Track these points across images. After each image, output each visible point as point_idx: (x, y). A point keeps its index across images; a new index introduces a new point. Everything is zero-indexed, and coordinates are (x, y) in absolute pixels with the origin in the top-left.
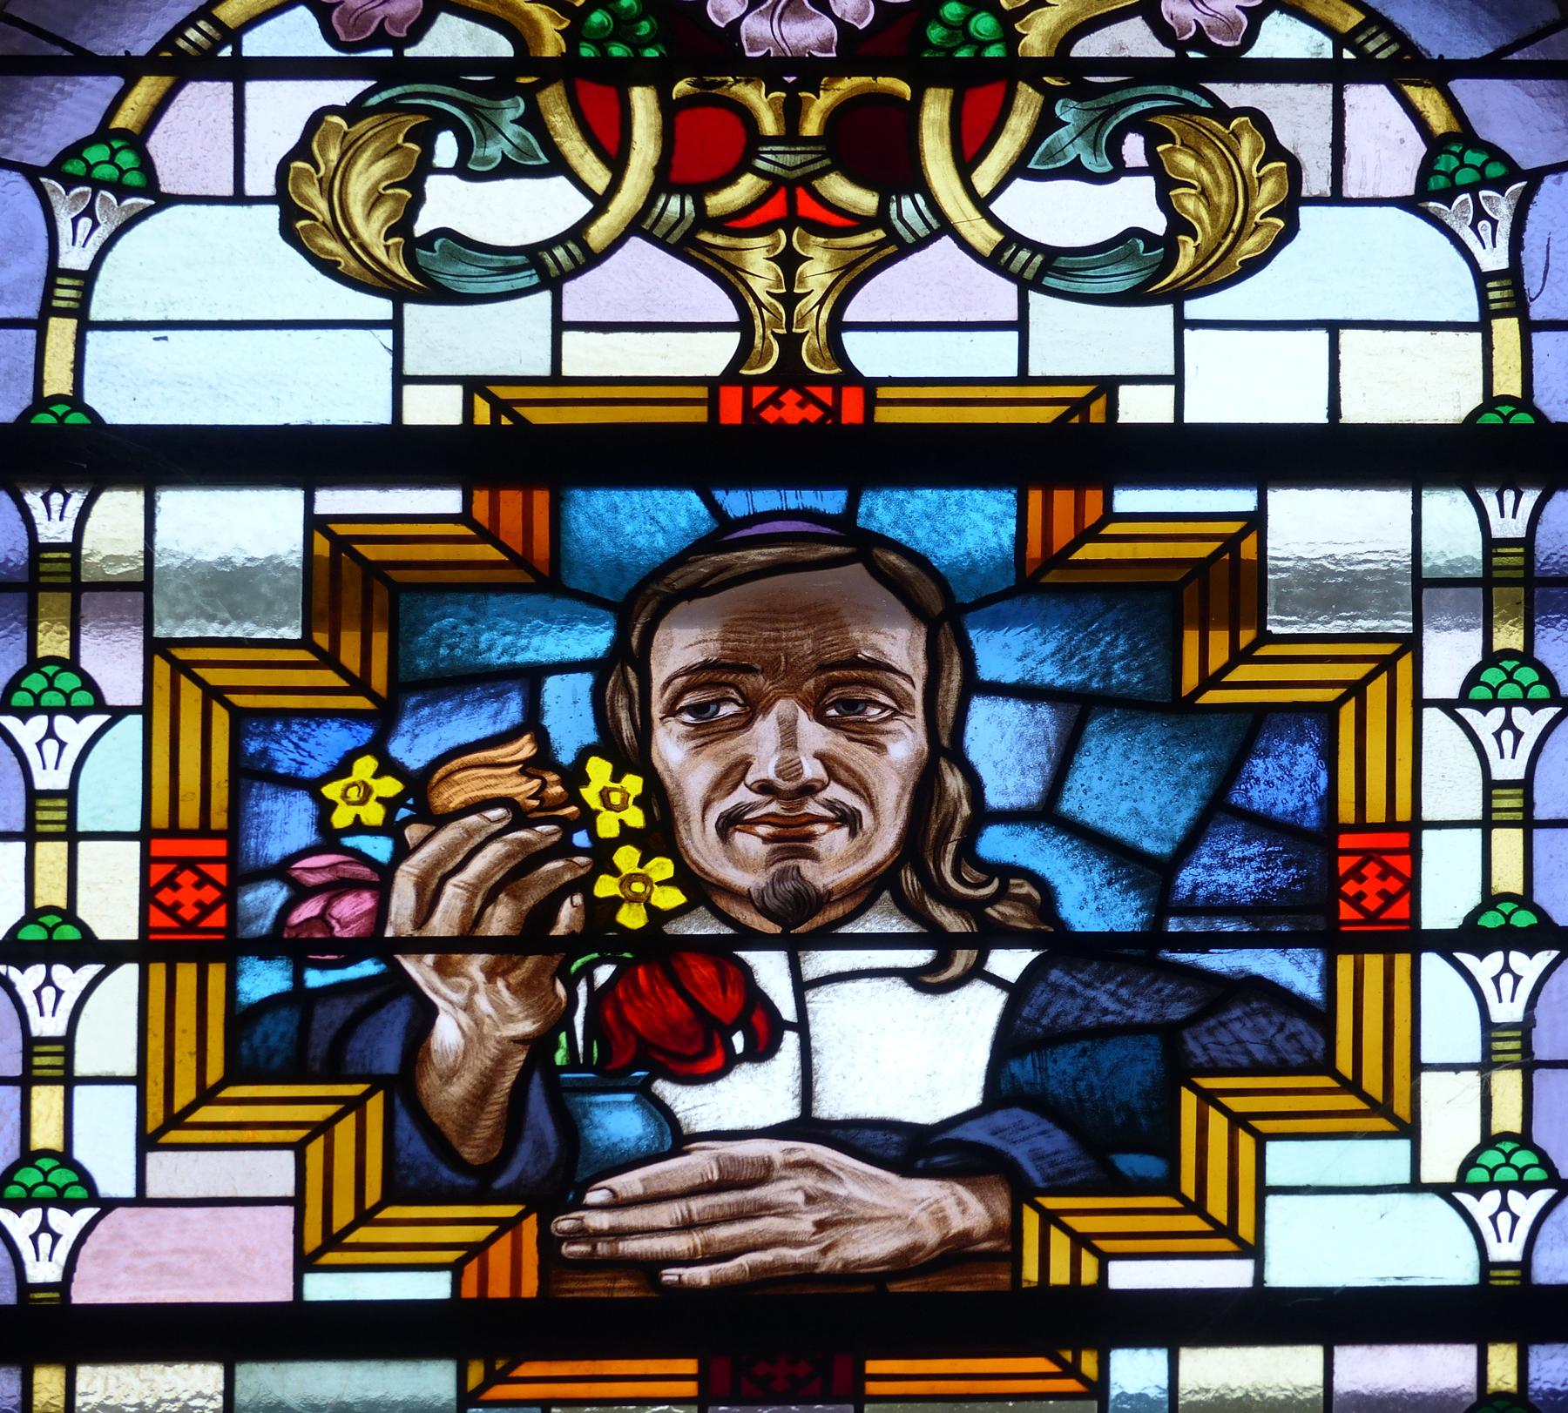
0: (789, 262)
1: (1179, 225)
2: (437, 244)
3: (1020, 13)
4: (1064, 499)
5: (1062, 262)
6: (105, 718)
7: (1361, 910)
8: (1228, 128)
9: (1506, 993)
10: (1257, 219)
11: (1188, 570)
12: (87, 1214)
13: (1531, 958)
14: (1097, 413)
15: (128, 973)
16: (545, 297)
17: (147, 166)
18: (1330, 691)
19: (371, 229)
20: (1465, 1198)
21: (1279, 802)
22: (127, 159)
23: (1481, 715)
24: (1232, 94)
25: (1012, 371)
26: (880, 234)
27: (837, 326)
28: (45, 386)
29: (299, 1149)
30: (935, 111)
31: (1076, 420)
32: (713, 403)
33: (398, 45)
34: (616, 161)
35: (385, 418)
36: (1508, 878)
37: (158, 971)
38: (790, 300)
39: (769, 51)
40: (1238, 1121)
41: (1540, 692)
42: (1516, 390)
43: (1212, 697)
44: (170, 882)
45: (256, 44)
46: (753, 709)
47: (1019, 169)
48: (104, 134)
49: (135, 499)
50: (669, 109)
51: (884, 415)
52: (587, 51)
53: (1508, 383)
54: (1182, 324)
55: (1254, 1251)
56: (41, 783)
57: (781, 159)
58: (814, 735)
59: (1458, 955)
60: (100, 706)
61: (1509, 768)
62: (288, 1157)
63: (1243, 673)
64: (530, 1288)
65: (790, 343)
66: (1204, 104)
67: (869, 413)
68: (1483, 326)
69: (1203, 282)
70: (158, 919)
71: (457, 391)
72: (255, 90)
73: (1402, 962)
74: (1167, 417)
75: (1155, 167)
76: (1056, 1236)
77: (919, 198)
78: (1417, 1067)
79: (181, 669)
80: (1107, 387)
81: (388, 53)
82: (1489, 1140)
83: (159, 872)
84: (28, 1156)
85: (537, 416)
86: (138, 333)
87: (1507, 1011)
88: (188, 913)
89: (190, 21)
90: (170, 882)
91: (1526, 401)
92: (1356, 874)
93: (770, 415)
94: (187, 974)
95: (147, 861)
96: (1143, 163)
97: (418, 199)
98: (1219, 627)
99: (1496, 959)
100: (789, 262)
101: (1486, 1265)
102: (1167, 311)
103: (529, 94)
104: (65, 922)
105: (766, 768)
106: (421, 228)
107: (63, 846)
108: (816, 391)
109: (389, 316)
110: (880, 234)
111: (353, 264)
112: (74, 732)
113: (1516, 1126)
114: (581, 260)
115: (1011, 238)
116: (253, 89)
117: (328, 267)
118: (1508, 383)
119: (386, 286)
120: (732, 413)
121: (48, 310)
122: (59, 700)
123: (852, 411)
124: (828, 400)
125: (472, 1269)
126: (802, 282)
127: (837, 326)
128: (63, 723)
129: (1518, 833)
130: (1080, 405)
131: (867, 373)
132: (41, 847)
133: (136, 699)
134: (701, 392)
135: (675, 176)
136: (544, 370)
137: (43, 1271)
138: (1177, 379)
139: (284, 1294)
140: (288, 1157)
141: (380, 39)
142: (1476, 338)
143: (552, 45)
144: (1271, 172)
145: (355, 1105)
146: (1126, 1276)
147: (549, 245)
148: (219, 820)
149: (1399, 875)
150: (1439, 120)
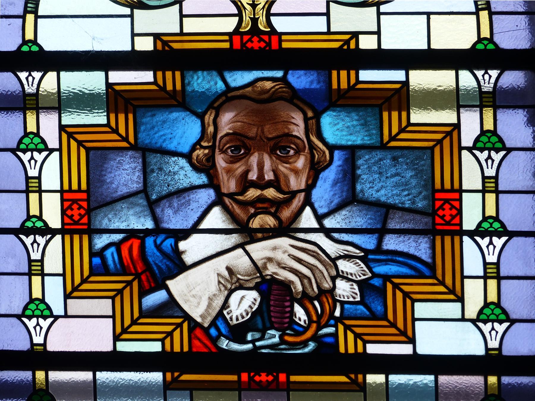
4: (344, 74)
6: (47, 152)
7: (444, 220)
9: (493, 337)
11: (384, 100)
12: (50, 320)
14: (352, 45)
15: (58, 238)
16: (177, 6)
18: (430, 143)
23: (480, 153)
25: (325, 30)
27: (269, 15)
28: (28, 129)
29: (113, 298)
31: (176, 374)
35: (129, 48)
36: (491, 211)
37: (67, 238)
40: (406, 295)
41: (503, 317)
42: (495, 300)
44: (70, 208)
46: (248, 153)
49: (55, 73)
51: (285, 45)
53: (485, 33)
54: (379, 14)
55: (412, 341)
56: (30, 175)
60: (52, 315)
61: (492, 258)
62: (110, 301)
63: (120, 286)
65: (255, 21)
67: (280, 45)
68: (476, 13)
71: (151, 38)
73: (457, 239)
74: (375, 46)
78: (463, 277)
79: (70, 136)
80: (355, 35)
83: (66, 204)
85: (175, 46)
90: (70, 208)
91: (491, 40)
93: (249, 45)
95: (63, 200)
98: (395, 110)
99: (487, 239)
101: (487, 349)
102: (375, 8)
107: (40, 277)
109: (130, 13)
112: (39, 157)
118: (485, 33)
120: (237, 45)
121: (26, 12)
123: (275, 46)
125: (168, 341)
127: (269, 15)
129: (494, 195)
130: (347, 42)
132: (33, 278)
134: (226, 38)
136: (178, 31)
137: (38, 340)
138: (378, 33)
142: (474, 17)
146: (372, 349)
148: (84, 186)
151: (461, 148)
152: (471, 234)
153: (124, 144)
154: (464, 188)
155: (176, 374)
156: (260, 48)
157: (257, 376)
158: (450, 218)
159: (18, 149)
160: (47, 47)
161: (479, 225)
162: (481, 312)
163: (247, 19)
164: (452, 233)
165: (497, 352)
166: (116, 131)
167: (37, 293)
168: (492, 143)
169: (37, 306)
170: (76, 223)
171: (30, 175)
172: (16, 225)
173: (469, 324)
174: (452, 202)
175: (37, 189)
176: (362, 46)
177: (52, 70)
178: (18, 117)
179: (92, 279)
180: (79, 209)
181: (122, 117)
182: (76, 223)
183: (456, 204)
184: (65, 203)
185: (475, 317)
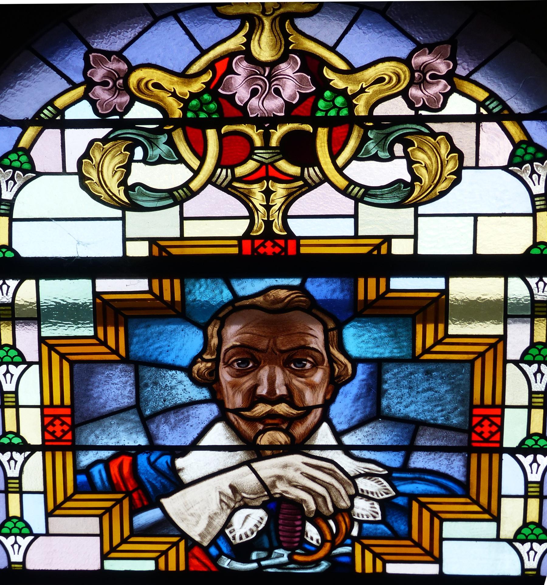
0: (268, 193)
1: (416, 178)
2: (136, 189)
3: (355, 95)
4: (372, 282)
5: (372, 192)
6: (25, 366)
8: (435, 140)
10: (446, 175)
12: (30, 538)
14: (384, 250)
17: (31, 161)
19: (113, 183)
20: (518, 545)
21: (358, 438)
22: (24, 158)
24: (437, 127)
25: (352, 234)
26: (301, 183)
27: (285, 217)
29: (100, 517)
30: (322, 134)
33: (122, 114)
34: (202, 157)
37: (49, 455)
38: (268, 207)
39: (258, 114)
43: (427, 357)
44: (51, 423)
45: (70, 115)
47: (355, 157)
48: (16, 149)
50: (221, 137)
51: (303, 250)
52: (190, 115)
54: (417, 216)
55: (439, 561)
57: (264, 155)
59: (517, 455)
63: (108, 504)
64: (182, 568)
65: (268, 224)
66: (427, 131)
67: (298, 250)
68: (534, 215)
69: (425, 199)
70: (48, 437)
71: (146, 243)
72: (69, 132)
74: (410, 251)
75: (407, 156)
76: (367, 553)
77: (316, 168)
79: (51, 348)
80: (388, 239)
81: (118, 117)
82: (526, 524)
83: (47, 420)
84: (9, 518)
85: (174, 251)
86: (31, 222)
87: (534, 477)
88: (59, 434)
89: (45, 107)
90: (51, 423)
92: (480, 424)
93: (261, 250)
94: (59, 455)
95: (43, 416)
96: (402, 154)
97: (128, 173)
100: (268, 193)
102: (412, 209)
103: (169, 132)
106: (131, 181)
108: (278, 241)
109: (121, 216)
110: (301, 183)
111: (107, 196)
113: (536, 520)
114: (189, 194)
115: (351, 182)
116: (68, 132)
117: (97, 198)
119: (117, 205)
122: (9, 359)
123: (291, 251)
124: (283, 245)
126: (273, 200)
127: (285, 217)
130: (378, 247)
131: (297, 234)
133: (36, 359)
134: (235, 242)
135: (222, 163)
136: (178, 235)
137: (17, 558)
138: (415, 237)
139: (452, 281)
140: (97, 519)
141: (114, 112)
142: (531, 219)
143: (177, 114)
144: (452, 157)
145: (119, 502)
147: (176, 189)
148: (67, 401)
149: (496, 425)
150: (518, 136)
151: (506, 361)
152: (512, 452)
153: (114, 357)
156: (274, 253)
160: (24, 254)
161: (523, 442)
163: (259, 221)
164: (491, 451)
165: (534, 573)
166: (104, 343)
169: (15, 524)
173: (505, 544)
179: (77, 497)
181: (111, 331)
183: (497, 420)
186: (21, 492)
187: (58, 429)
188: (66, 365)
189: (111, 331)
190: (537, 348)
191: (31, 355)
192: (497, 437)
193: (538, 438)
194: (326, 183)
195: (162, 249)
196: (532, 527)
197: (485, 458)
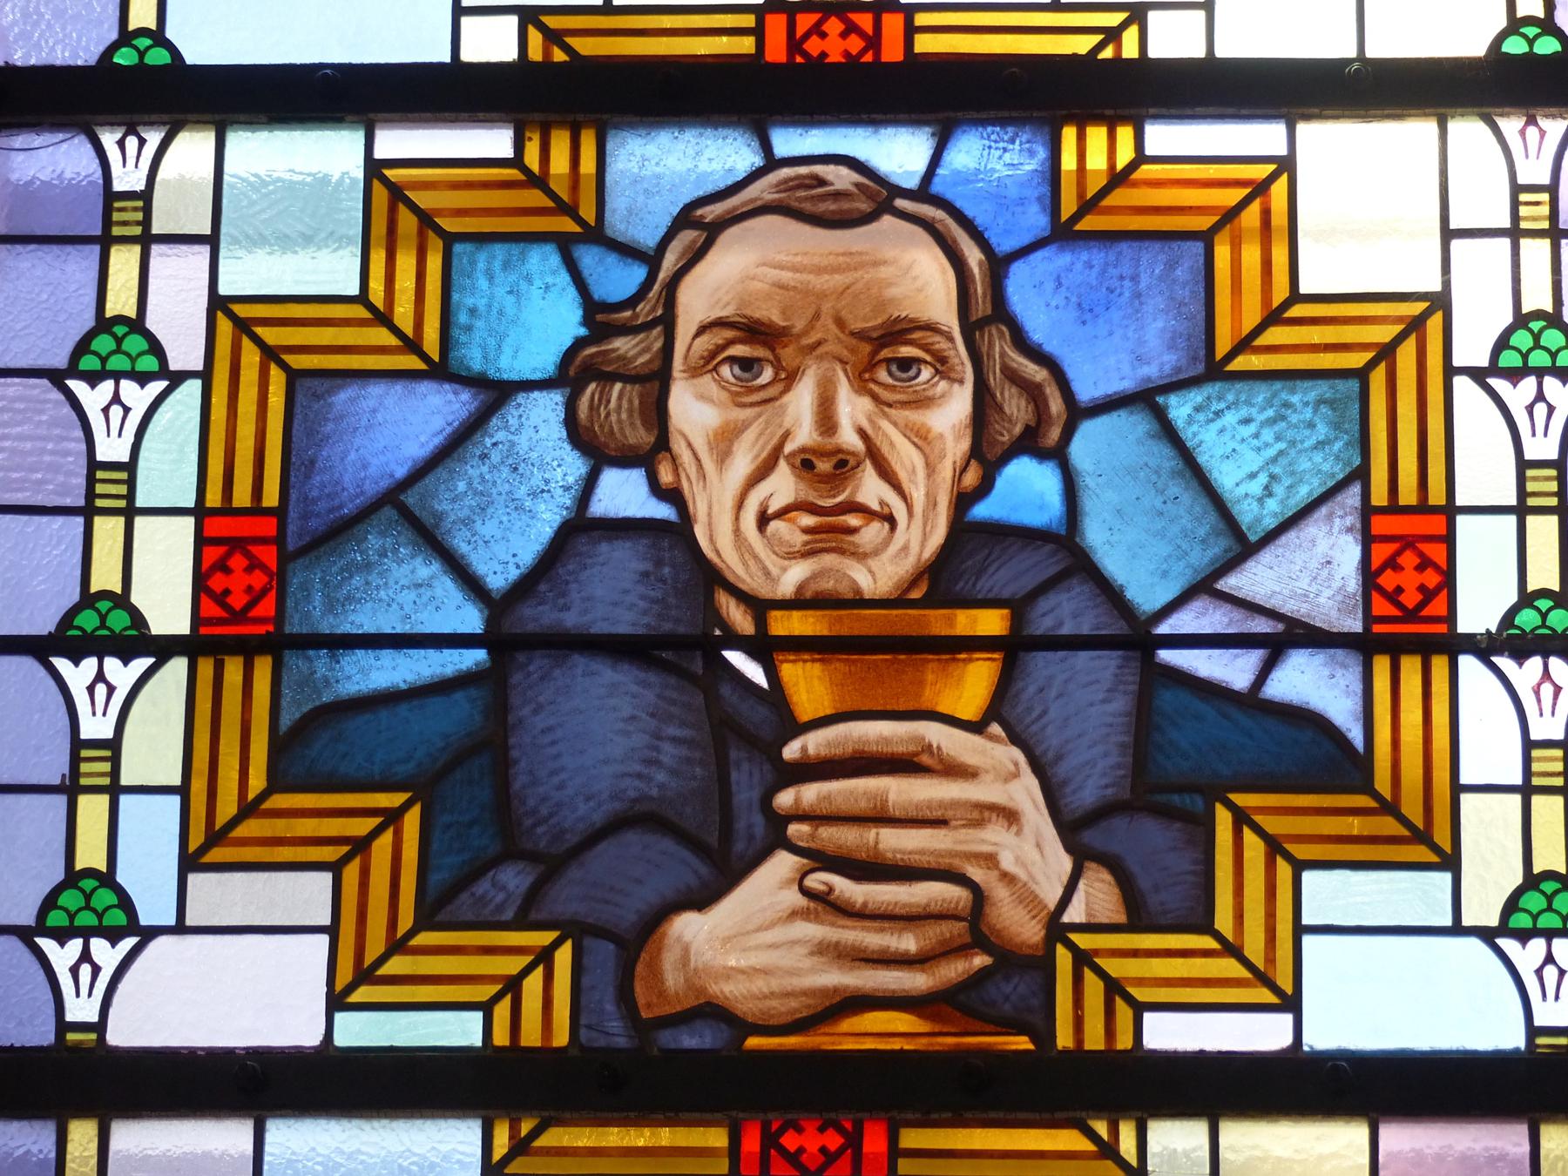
4: (1097, 136)
12: (158, 386)
13: (1564, 385)
15: (178, 667)
20: (1498, 384)
32: (758, 32)
37: (206, 667)
51: (925, 44)
55: (1291, 1003)
56: (102, 455)
58: (851, 409)
62: (1308, 877)
64: (561, 1038)
71: (512, 21)
73: (1440, 664)
78: (1457, 789)
79: (244, 327)
83: (212, 554)
85: (586, 47)
93: (814, 46)
95: (201, 541)
104: (117, 606)
105: (805, 434)
123: (892, 52)
125: (502, 1011)
128: (128, 388)
137: (81, 1009)
148: (271, 498)
151: (1450, 371)
152: (1485, 647)
153: (412, 362)
154: (1461, 500)
155: (526, 1128)
157: (854, 52)
158: (1420, 597)
159: (73, 371)
160: (190, 59)
161: (1508, 618)
162: (1512, 905)
164: (1426, 648)
167: (91, 855)
168: (128, 355)
169: (1550, 899)
170: (239, 617)
171: (102, 455)
172: (43, 623)
173: (1475, 943)
174: (255, 550)
175: (122, 504)
176: (1158, 49)
177: (200, 124)
178: (79, 265)
180: (1420, 568)
182: (239, 617)
184: (1375, 547)
185: (1494, 921)
186: (130, 512)
187: (238, 583)
188: (277, 377)
189: (406, 263)
190: (1524, 36)
191: (185, 352)
192: (1438, 607)
193: (1538, 30)
194: (193, 506)
195: (554, 37)
196: (1544, 604)
197: (1411, 667)
